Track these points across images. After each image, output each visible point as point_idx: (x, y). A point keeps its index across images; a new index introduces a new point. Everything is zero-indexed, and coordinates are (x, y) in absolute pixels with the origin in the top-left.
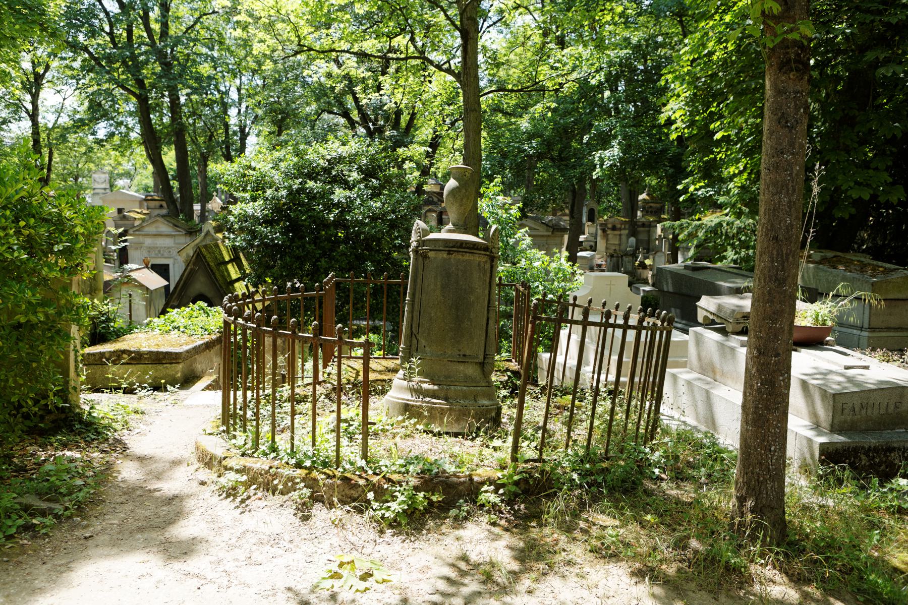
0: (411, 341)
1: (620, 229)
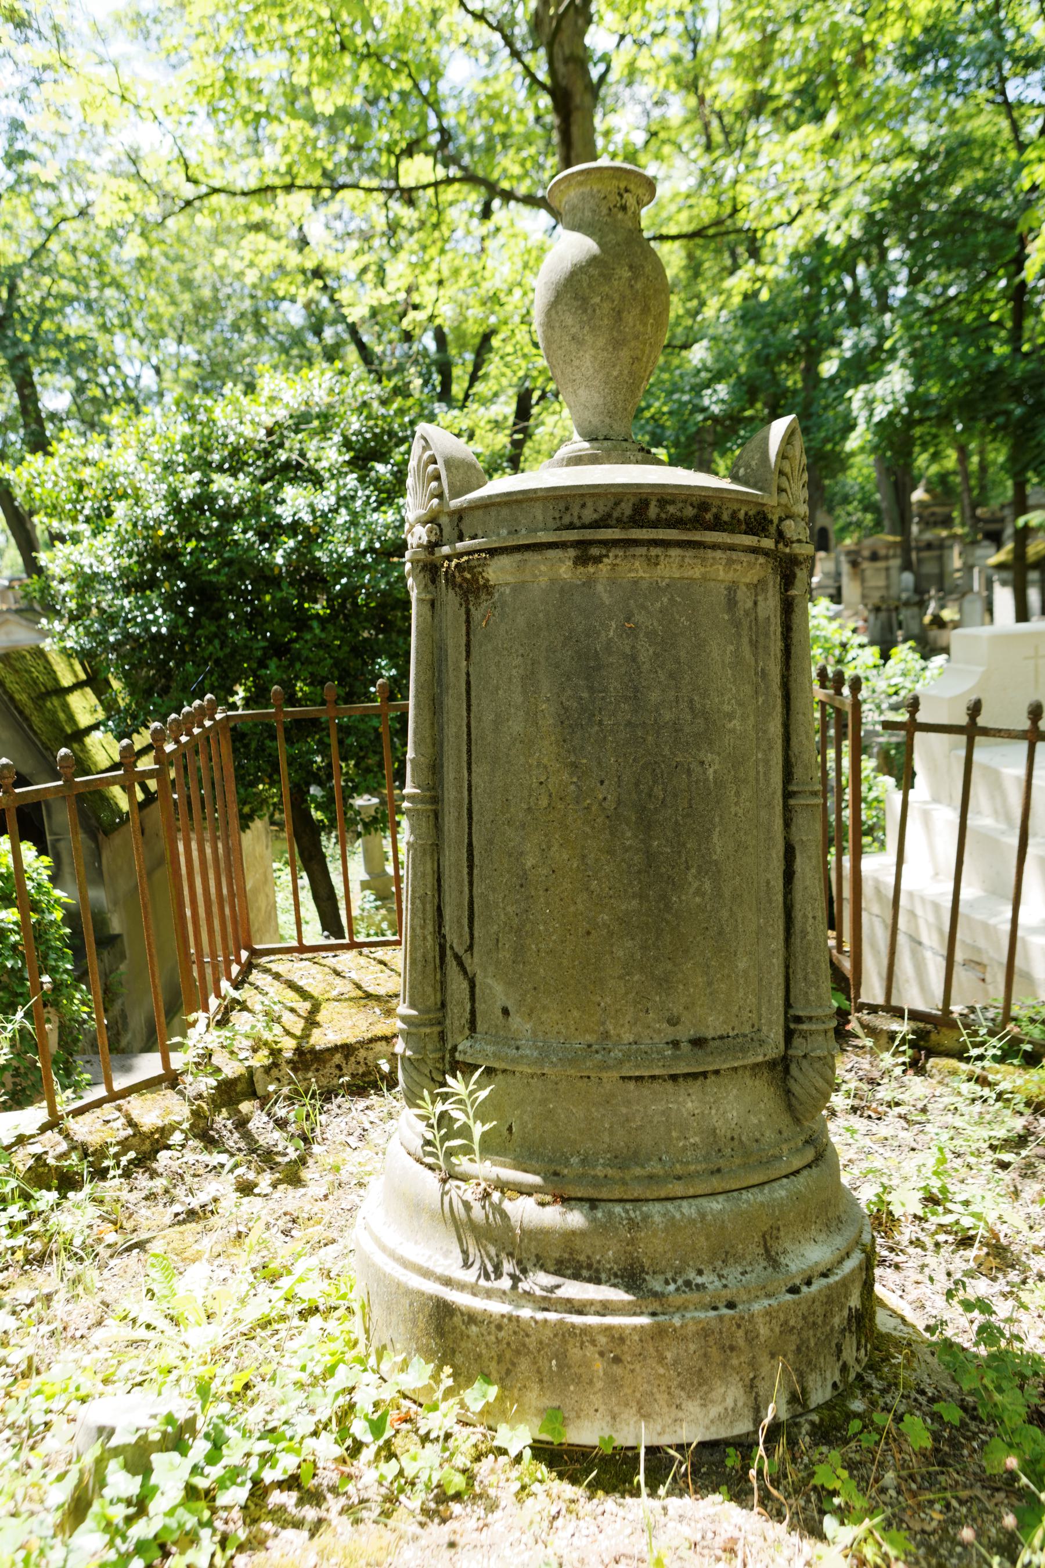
0: (443, 986)
1: (887, 558)
